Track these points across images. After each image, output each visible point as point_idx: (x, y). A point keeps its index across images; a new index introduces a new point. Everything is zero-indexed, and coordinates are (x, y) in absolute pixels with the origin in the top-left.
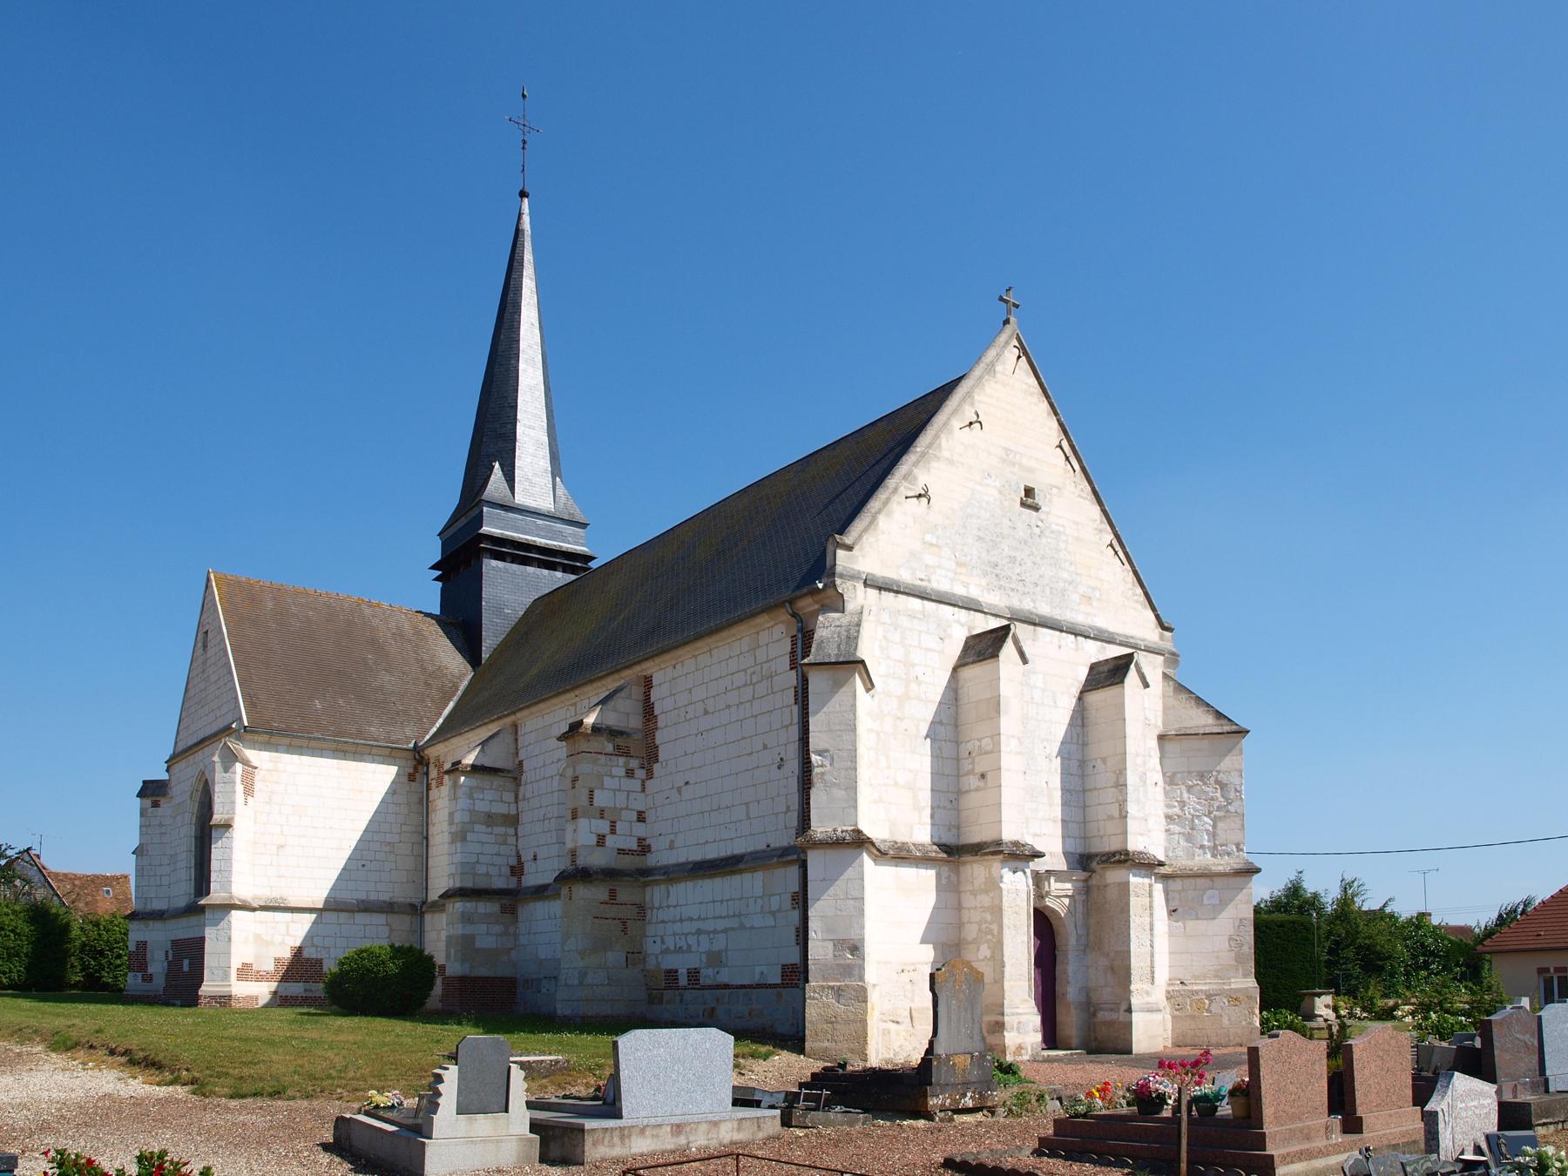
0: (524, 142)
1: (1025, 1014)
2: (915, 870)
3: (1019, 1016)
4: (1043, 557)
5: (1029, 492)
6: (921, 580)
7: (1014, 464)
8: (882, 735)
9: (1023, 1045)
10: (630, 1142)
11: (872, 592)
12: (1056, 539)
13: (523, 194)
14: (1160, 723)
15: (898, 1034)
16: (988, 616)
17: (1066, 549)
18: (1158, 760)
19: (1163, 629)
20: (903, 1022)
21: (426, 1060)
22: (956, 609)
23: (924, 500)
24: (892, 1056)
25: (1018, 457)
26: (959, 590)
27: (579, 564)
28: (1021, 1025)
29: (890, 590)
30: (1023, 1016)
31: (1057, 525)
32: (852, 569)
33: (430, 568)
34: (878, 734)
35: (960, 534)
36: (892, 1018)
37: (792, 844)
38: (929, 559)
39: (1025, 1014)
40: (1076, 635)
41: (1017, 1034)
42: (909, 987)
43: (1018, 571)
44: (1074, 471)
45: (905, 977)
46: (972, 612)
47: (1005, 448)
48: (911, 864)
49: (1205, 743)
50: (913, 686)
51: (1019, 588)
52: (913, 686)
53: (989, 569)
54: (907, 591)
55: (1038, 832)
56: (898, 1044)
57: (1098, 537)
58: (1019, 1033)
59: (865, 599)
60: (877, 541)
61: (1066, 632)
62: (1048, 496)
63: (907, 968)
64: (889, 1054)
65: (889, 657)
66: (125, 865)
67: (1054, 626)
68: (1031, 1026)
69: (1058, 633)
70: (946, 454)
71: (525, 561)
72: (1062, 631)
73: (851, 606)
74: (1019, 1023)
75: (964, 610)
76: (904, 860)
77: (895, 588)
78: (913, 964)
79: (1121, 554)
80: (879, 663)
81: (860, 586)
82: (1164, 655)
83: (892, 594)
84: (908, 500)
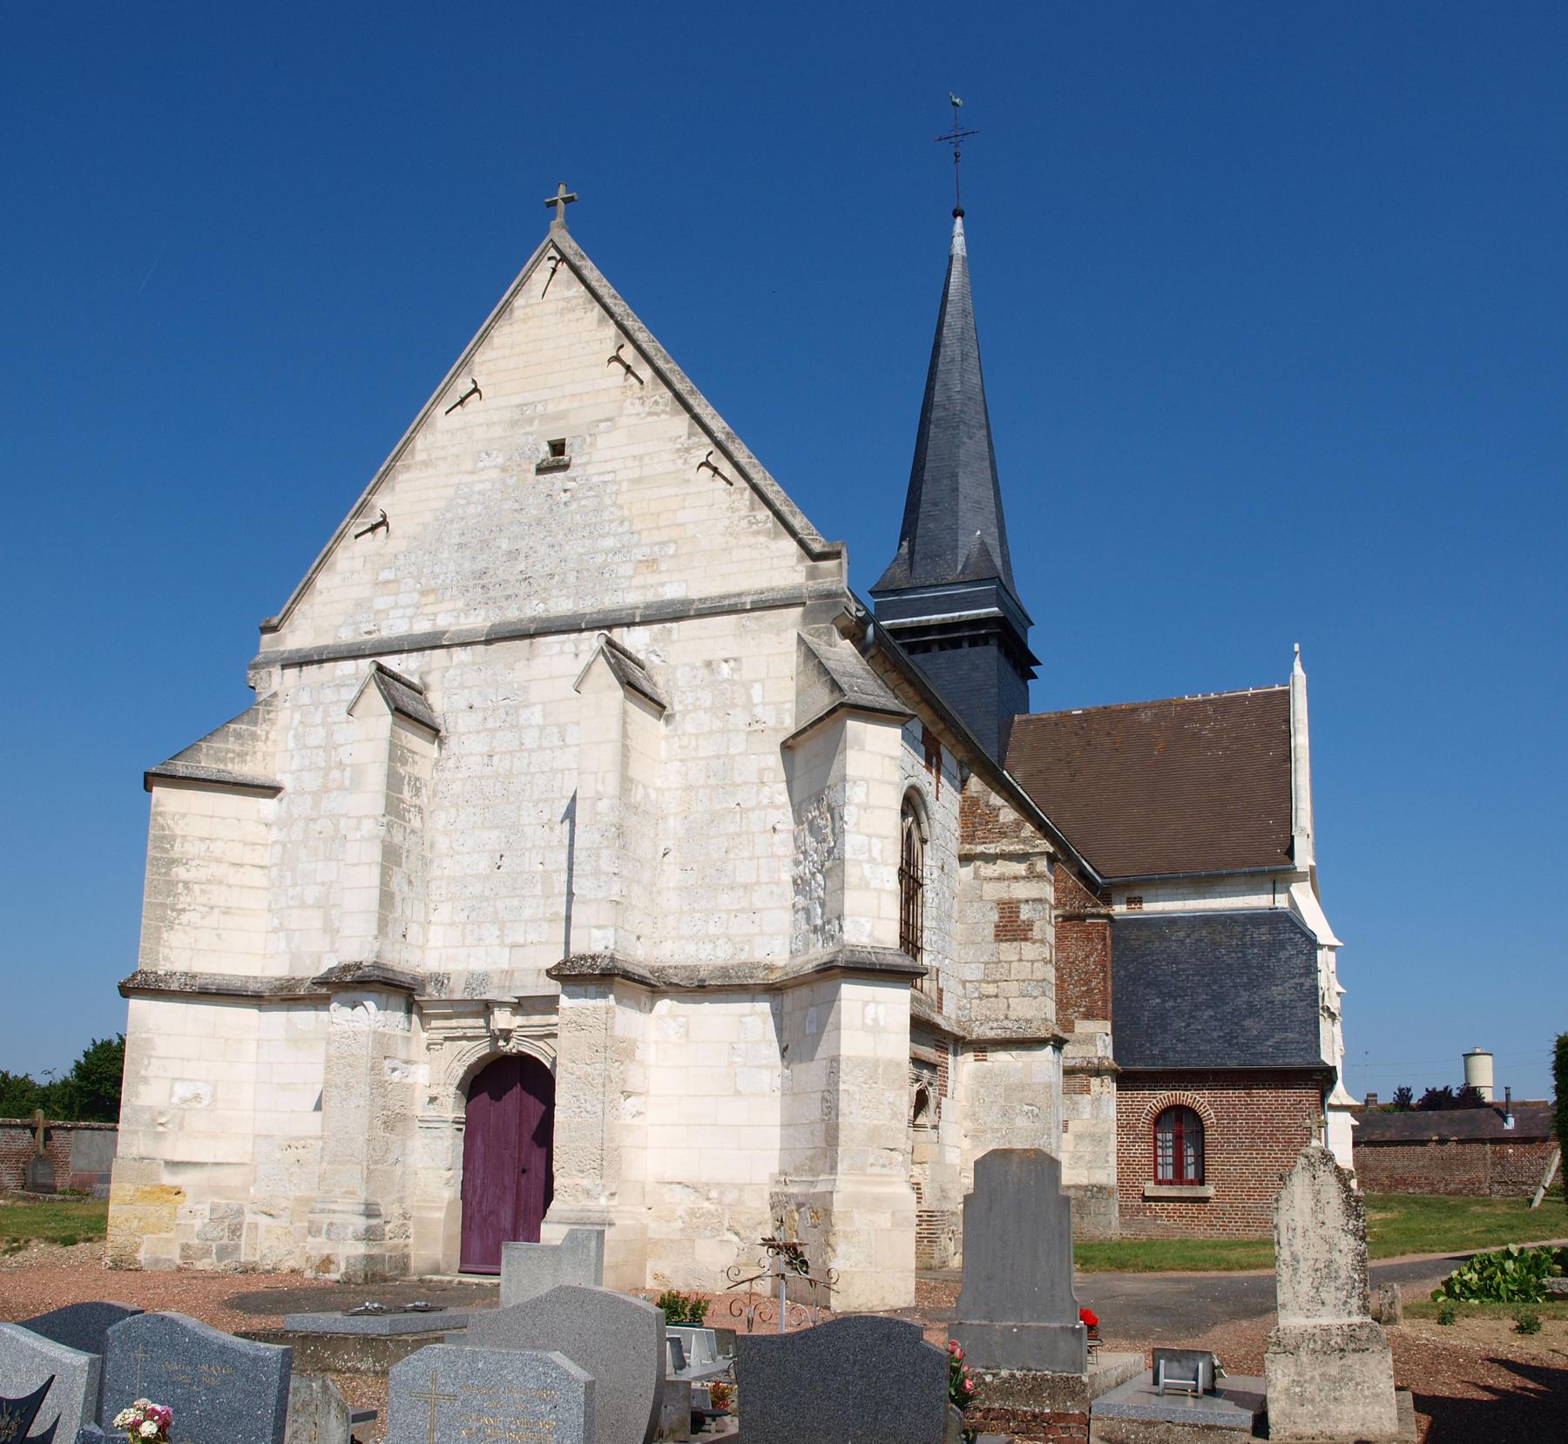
1: (342, 1212)
2: (313, 1013)
3: (331, 1215)
5: (558, 448)
6: (369, 633)
7: (530, 421)
8: (289, 845)
9: (332, 1257)
10: (941, 1330)
11: (292, 673)
12: (597, 496)
15: (268, 1231)
16: (454, 649)
17: (614, 504)
18: (783, 786)
19: (814, 560)
20: (281, 1216)
22: (404, 655)
24: (257, 1258)
25: (540, 408)
26: (422, 627)
27: (983, 632)
28: (333, 1229)
29: (312, 663)
30: (337, 1215)
31: (600, 474)
32: (284, 652)
33: (1040, 664)
34: (284, 845)
35: (430, 553)
36: (264, 1209)
38: (381, 603)
39: (342, 1212)
41: (326, 1240)
42: (296, 1169)
43: (522, 567)
44: (641, 382)
46: (427, 652)
47: (517, 406)
48: (307, 1006)
51: (517, 592)
53: (472, 583)
54: (331, 656)
55: (521, 941)
56: (267, 1244)
57: (681, 461)
58: (329, 1238)
59: (281, 683)
60: (312, 606)
61: (587, 629)
62: (588, 439)
63: (294, 1143)
64: (254, 1255)
65: (305, 747)
67: (564, 628)
68: (350, 1230)
69: (574, 636)
70: (420, 456)
71: (956, 644)
72: (581, 631)
74: (331, 1224)
75: (415, 654)
76: (300, 1002)
77: (316, 658)
78: (303, 1139)
79: (727, 469)
80: (292, 757)
82: (804, 604)
83: (315, 666)
84: (359, 539)
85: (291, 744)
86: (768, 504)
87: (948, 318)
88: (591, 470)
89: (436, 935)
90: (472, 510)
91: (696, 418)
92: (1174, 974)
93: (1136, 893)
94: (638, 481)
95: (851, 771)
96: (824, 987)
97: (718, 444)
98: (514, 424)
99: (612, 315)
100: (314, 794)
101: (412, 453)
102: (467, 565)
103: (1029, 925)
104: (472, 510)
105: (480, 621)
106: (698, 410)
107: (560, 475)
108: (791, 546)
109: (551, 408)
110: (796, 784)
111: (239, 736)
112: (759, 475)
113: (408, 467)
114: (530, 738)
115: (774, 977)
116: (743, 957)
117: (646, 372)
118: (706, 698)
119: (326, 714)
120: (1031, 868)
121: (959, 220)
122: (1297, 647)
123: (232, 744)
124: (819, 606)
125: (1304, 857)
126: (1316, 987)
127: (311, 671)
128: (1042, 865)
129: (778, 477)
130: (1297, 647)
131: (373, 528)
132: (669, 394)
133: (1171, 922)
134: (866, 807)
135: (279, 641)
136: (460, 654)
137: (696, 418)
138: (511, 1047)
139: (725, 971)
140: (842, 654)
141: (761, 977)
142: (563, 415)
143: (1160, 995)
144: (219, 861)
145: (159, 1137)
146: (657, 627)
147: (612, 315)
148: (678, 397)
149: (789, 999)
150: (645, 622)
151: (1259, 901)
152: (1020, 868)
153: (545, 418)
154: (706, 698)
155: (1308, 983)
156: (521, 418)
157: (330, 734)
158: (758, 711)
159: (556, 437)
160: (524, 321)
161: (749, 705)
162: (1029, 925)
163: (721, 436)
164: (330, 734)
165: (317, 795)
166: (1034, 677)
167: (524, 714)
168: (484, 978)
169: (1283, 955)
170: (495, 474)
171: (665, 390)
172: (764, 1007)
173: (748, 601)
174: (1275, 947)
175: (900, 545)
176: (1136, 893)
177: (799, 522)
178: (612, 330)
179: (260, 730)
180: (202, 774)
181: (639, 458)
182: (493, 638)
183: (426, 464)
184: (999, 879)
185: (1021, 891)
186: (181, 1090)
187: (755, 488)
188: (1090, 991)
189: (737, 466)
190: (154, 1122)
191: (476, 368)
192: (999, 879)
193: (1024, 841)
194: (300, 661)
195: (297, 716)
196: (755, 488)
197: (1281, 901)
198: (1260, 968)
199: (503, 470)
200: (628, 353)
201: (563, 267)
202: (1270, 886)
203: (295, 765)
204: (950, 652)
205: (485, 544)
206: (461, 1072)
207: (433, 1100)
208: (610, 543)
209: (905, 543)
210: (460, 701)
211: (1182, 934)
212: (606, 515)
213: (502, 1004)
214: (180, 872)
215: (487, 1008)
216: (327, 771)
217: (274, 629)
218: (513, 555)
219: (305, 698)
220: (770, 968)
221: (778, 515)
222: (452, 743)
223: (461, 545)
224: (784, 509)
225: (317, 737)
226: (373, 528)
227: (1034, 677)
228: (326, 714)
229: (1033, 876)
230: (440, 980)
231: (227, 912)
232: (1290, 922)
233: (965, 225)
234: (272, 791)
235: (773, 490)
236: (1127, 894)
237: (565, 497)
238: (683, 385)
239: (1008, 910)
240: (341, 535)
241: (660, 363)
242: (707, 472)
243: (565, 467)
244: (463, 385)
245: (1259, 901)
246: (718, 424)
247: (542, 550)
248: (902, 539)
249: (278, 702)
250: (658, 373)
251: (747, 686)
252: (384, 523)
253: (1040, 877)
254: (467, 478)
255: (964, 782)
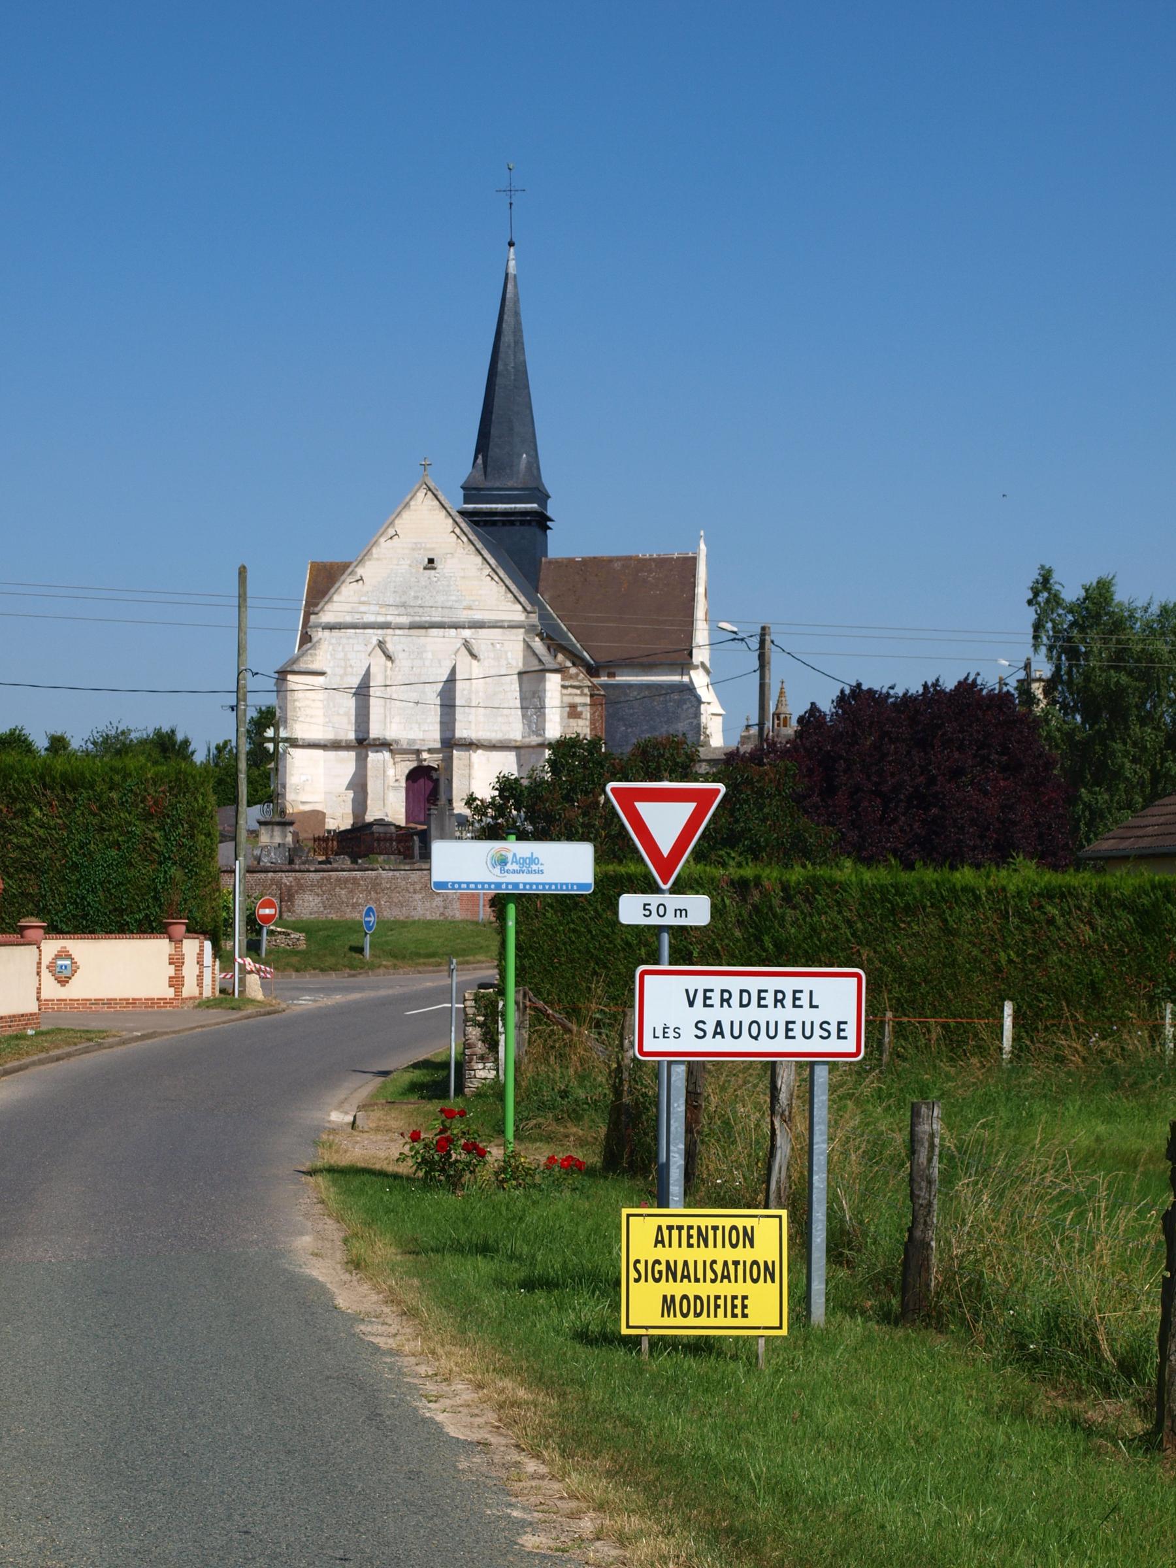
0: (511, 204)
4: (437, 592)
7: (420, 549)
13: (511, 244)
14: (521, 664)
21: (1108, 988)
23: (361, 582)
26: (381, 619)
37: (588, 723)
40: (456, 628)
45: (341, 799)
49: (534, 675)
50: (349, 669)
52: (349, 669)
66: (370, 754)
70: (375, 556)
71: (512, 523)
73: (315, 639)
79: (496, 578)
81: (320, 629)
85: (329, 657)
86: (512, 592)
87: (506, 317)
88: (445, 571)
89: (394, 726)
90: (398, 579)
91: (484, 559)
92: (632, 715)
93: (612, 670)
94: (464, 577)
95: (547, 688)
96: (539, 750)
97: (493, 569)
98: (413, 549)
99: (450, 515)
100: (341, 676)
101: (372, 554)
102: (398, 599)
103: (581, 713)
104: (398, 579)
105: (405, 620)
106: (485, 556)
107: (433, 571)
108: (519, 607)
109: (428, 546)
110: (524, 686)
111: (311, 655)
112: (508, 582)
113: (370, 560)
114: (427, 663)
115: (518, 744)
116: (506, 737)
117: (465, 539)
118: (492, 655)
119: (343, 648)
120: (582, 692)
121: (512, 249)
122: (702, 533)
123: (309, 658)
124: (530, 629)
125: (701, 655)
126: (699, 724)
127: (336, 633)
128: (586, 691)
129: (515, 582)
130: (702, 533)
131: (357, 581)
132: (473, 548)
133: (630, 686)
134: (551, 698)
135: (320, 618)
136: (398, 632)
137: (484, 559)
138: (425, 764)
139: (501, 741)
140: (538, 645)
141: (513, 744)
142: (433, 549)
143: (625, 725)
144: (308, 699)
145: (298, 793)
146: (473, 630)
147: (450, 515)
148: (477, 550)
149: (523, 751)
150: (470, 628)
151: (676, 678)
152: (578, 692)
153: (426, 549)
154: (492, 655)
155: (695, 722)
156: (416, 547)
157: (346, 655)
158: (510, 661)
159: (431, 557)
160: (415, 510)
161: (507, 659)
162: (581, 713)
163: (494, 566)
164: (346, 655)
165: (342, 677)
166: (550, 528)
167: (425, 655)
168: (414, 741)
169: (685, 707)
170: (407, 567)
171: (471, 546)
172: (514, 753)
173: (506, 624)
174: (680, 703)
175: (476, 458)
176: (612, 670)
177: (522, 599)
178: (451, 521)
179: (317, 652)
180: (302, 670)
181: (463, 569)
182: (413, 626)
183: (378, 559)
184: (570, 695)
185: (578, 700)
186: (303, 778)
187: (507, 586)
188: (595, 728)
189: (500, 578)
190: (296, 789)
191: (396, 526)
192: (570, 695)
193: (580, 681)
194: (331, 627)
195: (331, 647)
196: (507, 586)
197: (686, 679)
198: (673, 713)
199: (410, 566)
200: (457, 530)
201: (429, 493)
202: (680, 670)
203: (331, 665)
204: (507, 528)
205: (405, 593)
206: (407, 772)
207: (397, 780)
208: (454, 598)
209: (480, 457)
210: (400, 647)
211: (635, 693)
212: (452, 588)
213: (424, 751)
214: (297, 704)
215: (418, 752)
216: (345, 668)
217: (317, 614)
218: (416, 598)
219: (334, 641)
220: (516, 741)
221: (515, 597)
222: (397, 662)
223: (395, 592)
224: (517, 595)
225: (341, 655)
226: (357, 581)
227: (550, 528)
228: (343, 648)
229: (583, 694)
230: (397, 742)
231: (311, 717)
232: (690, 689)
233: (515, 254)
234: (322, 674)
235: (513, 587)
236: (607, 671)
237: (435, 579)
238: (479, 545)
239: (573, 706)
240: (344, 582)
241: (470, 537)
242: (489, 578)
243: (434, 569)
244: (391, 532)
245: (676, 678)
246: (492, 561)
247: (428, 598)
248: (478, 451)
249: (322, 641)
250: (469, 540)
251: (506, 652)
252: (361, 579)
253: (586, 695)
254: (395, 567)
255: (555, 656)
